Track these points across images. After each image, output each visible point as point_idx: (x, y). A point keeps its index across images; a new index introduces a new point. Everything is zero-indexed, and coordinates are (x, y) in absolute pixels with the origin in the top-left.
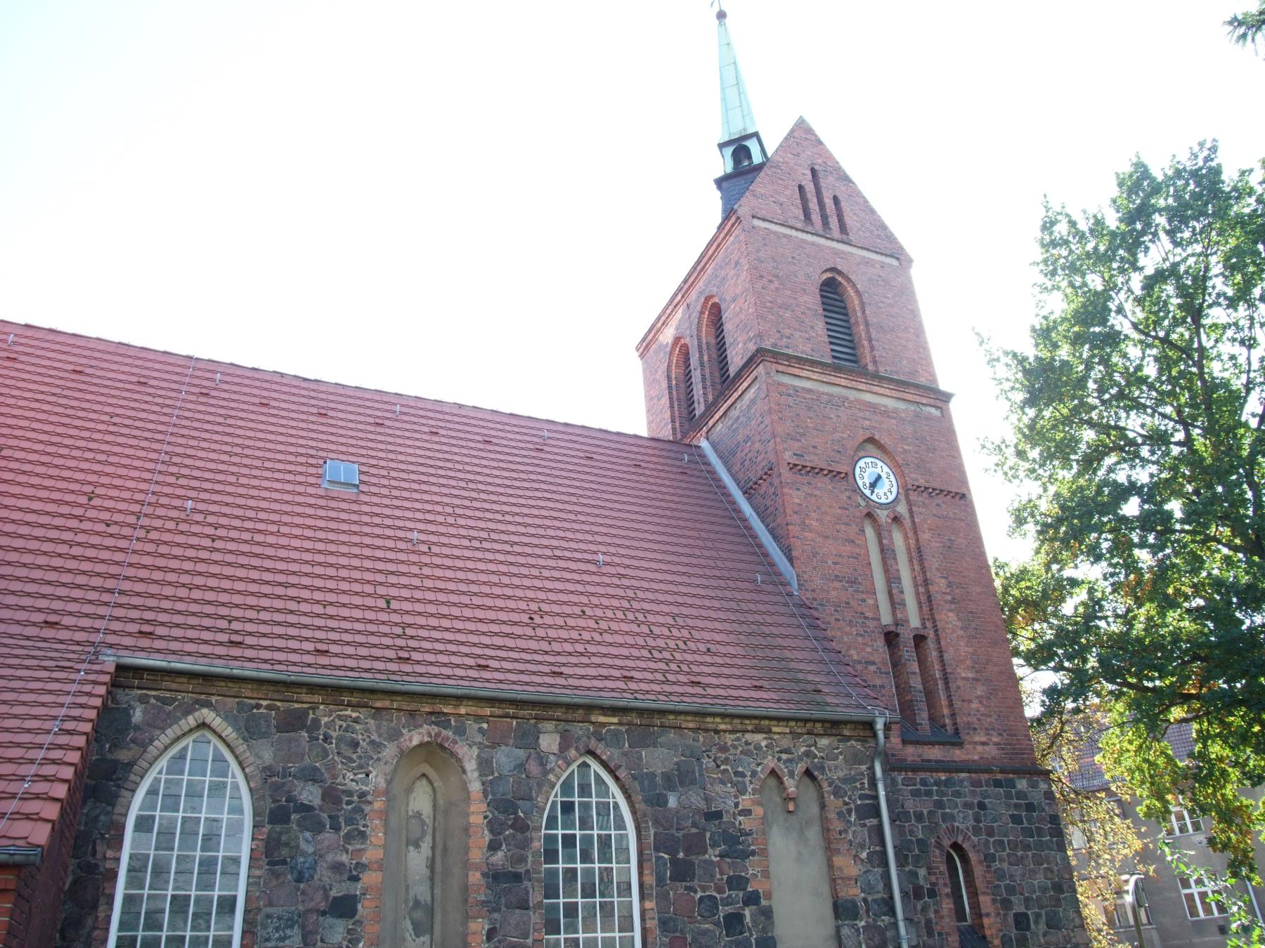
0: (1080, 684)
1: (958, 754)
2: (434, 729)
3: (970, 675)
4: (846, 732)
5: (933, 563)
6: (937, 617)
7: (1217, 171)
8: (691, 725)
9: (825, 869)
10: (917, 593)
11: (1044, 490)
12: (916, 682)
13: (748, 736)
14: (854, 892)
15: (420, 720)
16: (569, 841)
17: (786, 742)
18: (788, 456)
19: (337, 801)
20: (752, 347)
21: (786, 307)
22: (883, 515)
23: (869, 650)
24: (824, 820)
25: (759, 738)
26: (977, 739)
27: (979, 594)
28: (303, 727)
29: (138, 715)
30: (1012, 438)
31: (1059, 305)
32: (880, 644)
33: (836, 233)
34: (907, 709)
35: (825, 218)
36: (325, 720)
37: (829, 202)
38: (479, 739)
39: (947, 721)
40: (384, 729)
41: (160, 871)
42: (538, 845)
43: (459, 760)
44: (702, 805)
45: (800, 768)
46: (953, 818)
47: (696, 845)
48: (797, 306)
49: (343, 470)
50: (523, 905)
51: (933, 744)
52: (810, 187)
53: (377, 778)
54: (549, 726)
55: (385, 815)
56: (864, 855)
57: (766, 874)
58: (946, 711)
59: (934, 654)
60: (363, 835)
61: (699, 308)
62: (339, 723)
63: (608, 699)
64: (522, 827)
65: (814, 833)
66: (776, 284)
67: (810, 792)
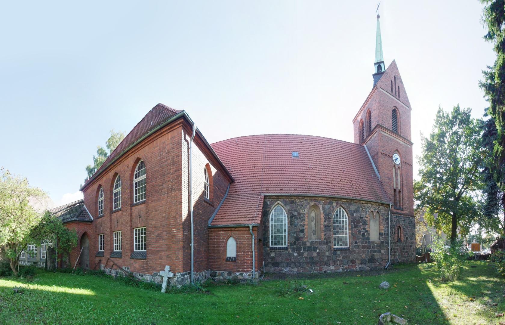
0: (423, 204)
1: (402, 212)
5: (404, 178)
7: (469, 116)
11: (425, 169)
12: (398, 199)
14: (383, 232)
16: (337, 221)
17: (375, 206)
20: (377, 124)
21: (385, 114)
22: (397, 166)
24: (379, 220)
25: (370, 205)
29: (269, 203)
30: (422, 156)
31: (437, 131)
32: (393, 191)
33: (397, 97)
34: (395, 203)
35: (396, 92)
37: (397, 87)
41: (275, 226)
42: (332, 221)
47: (358, 222)
49: (296, 154)
50: (330, 231)
52: (393, 82)
53: (306, 211)
55: (308, 216)
60: (304, 220)
63: (344, 197)
64: (330, 218)
65: (377, 222)
67: (378, 215)
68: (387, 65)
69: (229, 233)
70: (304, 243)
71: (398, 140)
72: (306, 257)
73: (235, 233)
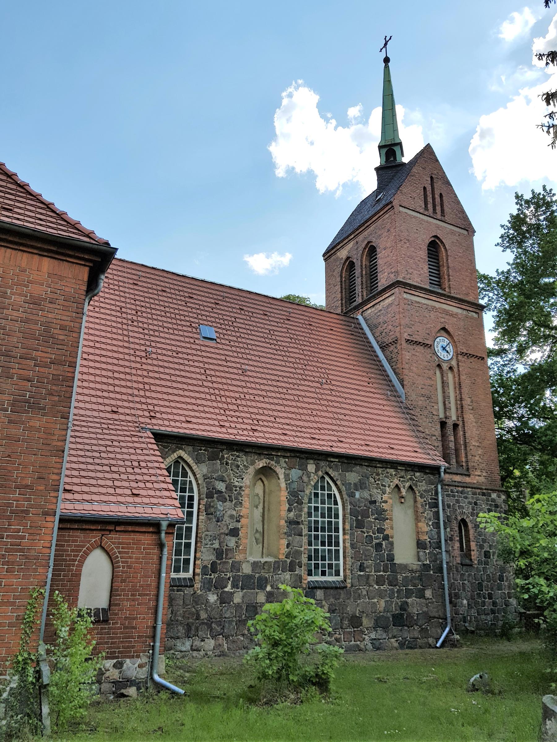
1: (467, 480)
2: (268, 461)
3: (477, 444)
4: (427, 471)
6: (465, 416)
8: (366, 464)
9: (414, 527)
10: (456, 404)
12: (452, 445)
13: (388, 470)
15: (262, 457)
18: (406, 336)
19: (231, 490)
22: (445, 366)
23: (433, 429)
24: (415, 507)
26: (476, 473)
27: (485, 406)
28: (218, 459)
32: (438, 427)
33: (439, 217)
36: (226, 456)
38: (285, 465)
39: (464, 464)
40: (249, 460)
43: (277, 474)
44: (369, 497)
45: (407, 485)
46: (463, 508)
48: (417, 257)
51: (457, 474)
54: (312, 461)
56: (430, 523)
57: (392, 528)
58: (464, 460)
59: (461, 433)
61: (363, 246)
62: (231, 457)
64: (300, 503)
65: (410, 512)
66: (408, 245)
68: (408, 155)
69: (94, 537)
70: (236, 566)
71: (445, 306)
72: (238, 606)
73: (113, 540)
